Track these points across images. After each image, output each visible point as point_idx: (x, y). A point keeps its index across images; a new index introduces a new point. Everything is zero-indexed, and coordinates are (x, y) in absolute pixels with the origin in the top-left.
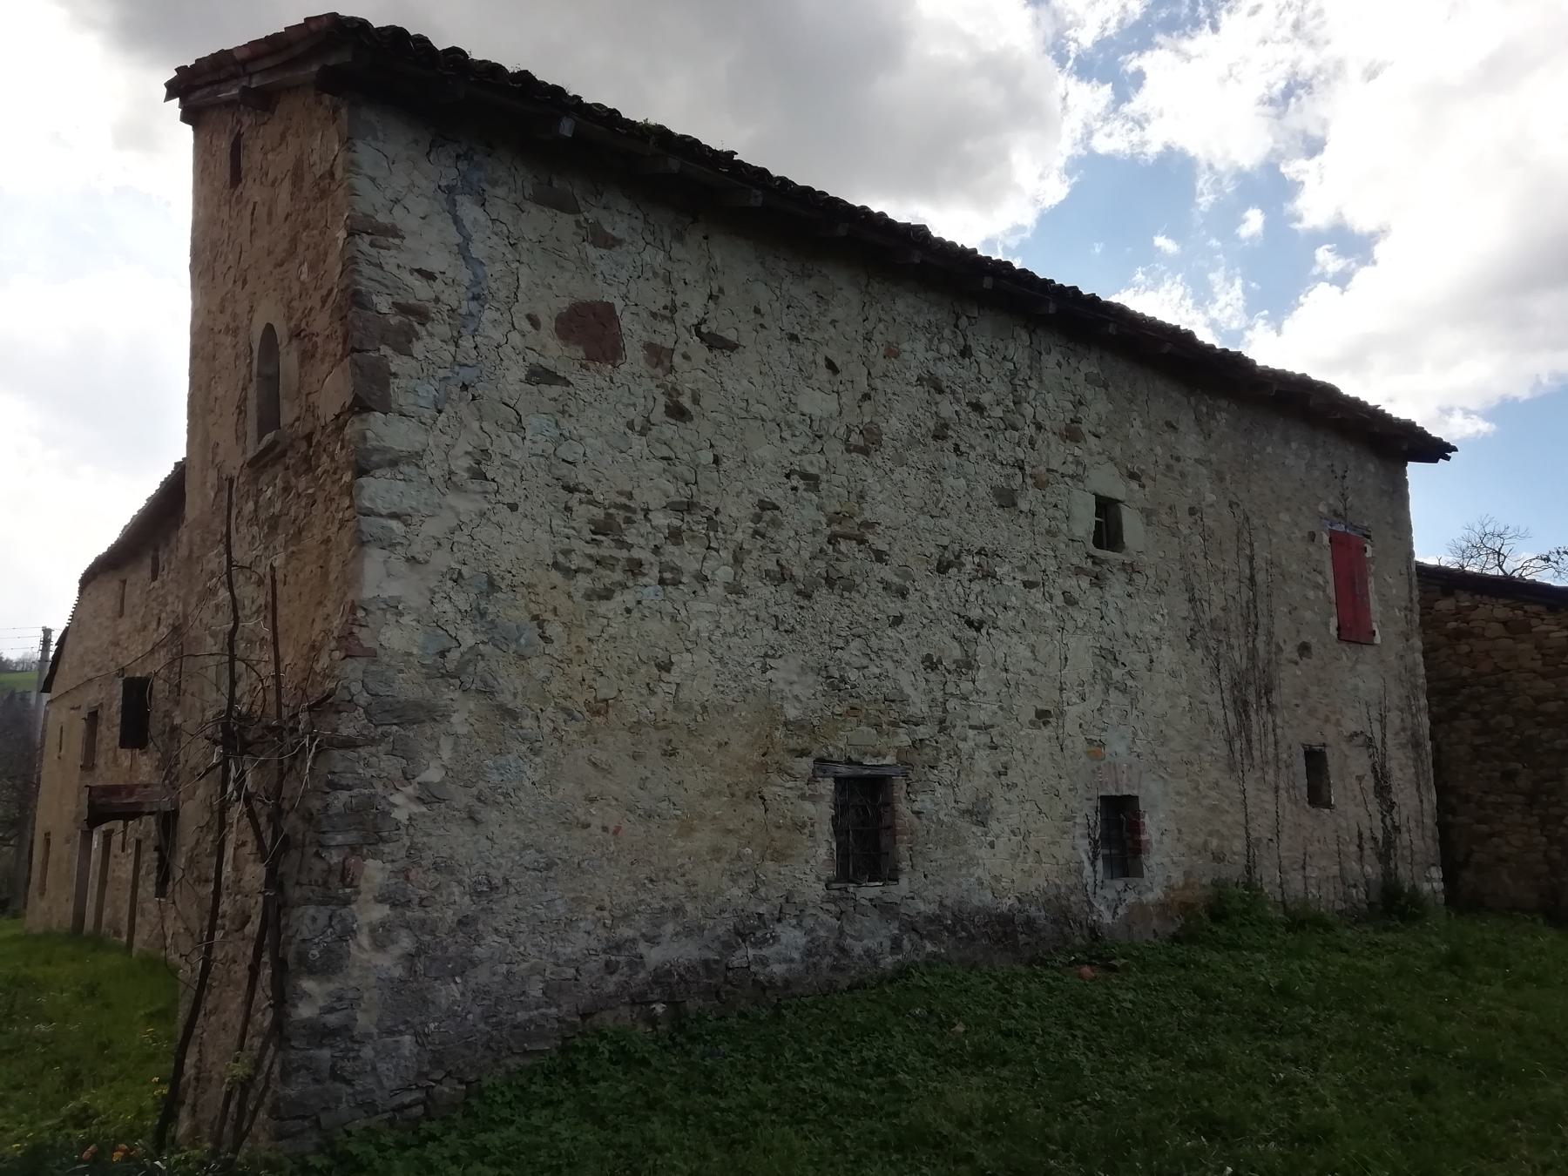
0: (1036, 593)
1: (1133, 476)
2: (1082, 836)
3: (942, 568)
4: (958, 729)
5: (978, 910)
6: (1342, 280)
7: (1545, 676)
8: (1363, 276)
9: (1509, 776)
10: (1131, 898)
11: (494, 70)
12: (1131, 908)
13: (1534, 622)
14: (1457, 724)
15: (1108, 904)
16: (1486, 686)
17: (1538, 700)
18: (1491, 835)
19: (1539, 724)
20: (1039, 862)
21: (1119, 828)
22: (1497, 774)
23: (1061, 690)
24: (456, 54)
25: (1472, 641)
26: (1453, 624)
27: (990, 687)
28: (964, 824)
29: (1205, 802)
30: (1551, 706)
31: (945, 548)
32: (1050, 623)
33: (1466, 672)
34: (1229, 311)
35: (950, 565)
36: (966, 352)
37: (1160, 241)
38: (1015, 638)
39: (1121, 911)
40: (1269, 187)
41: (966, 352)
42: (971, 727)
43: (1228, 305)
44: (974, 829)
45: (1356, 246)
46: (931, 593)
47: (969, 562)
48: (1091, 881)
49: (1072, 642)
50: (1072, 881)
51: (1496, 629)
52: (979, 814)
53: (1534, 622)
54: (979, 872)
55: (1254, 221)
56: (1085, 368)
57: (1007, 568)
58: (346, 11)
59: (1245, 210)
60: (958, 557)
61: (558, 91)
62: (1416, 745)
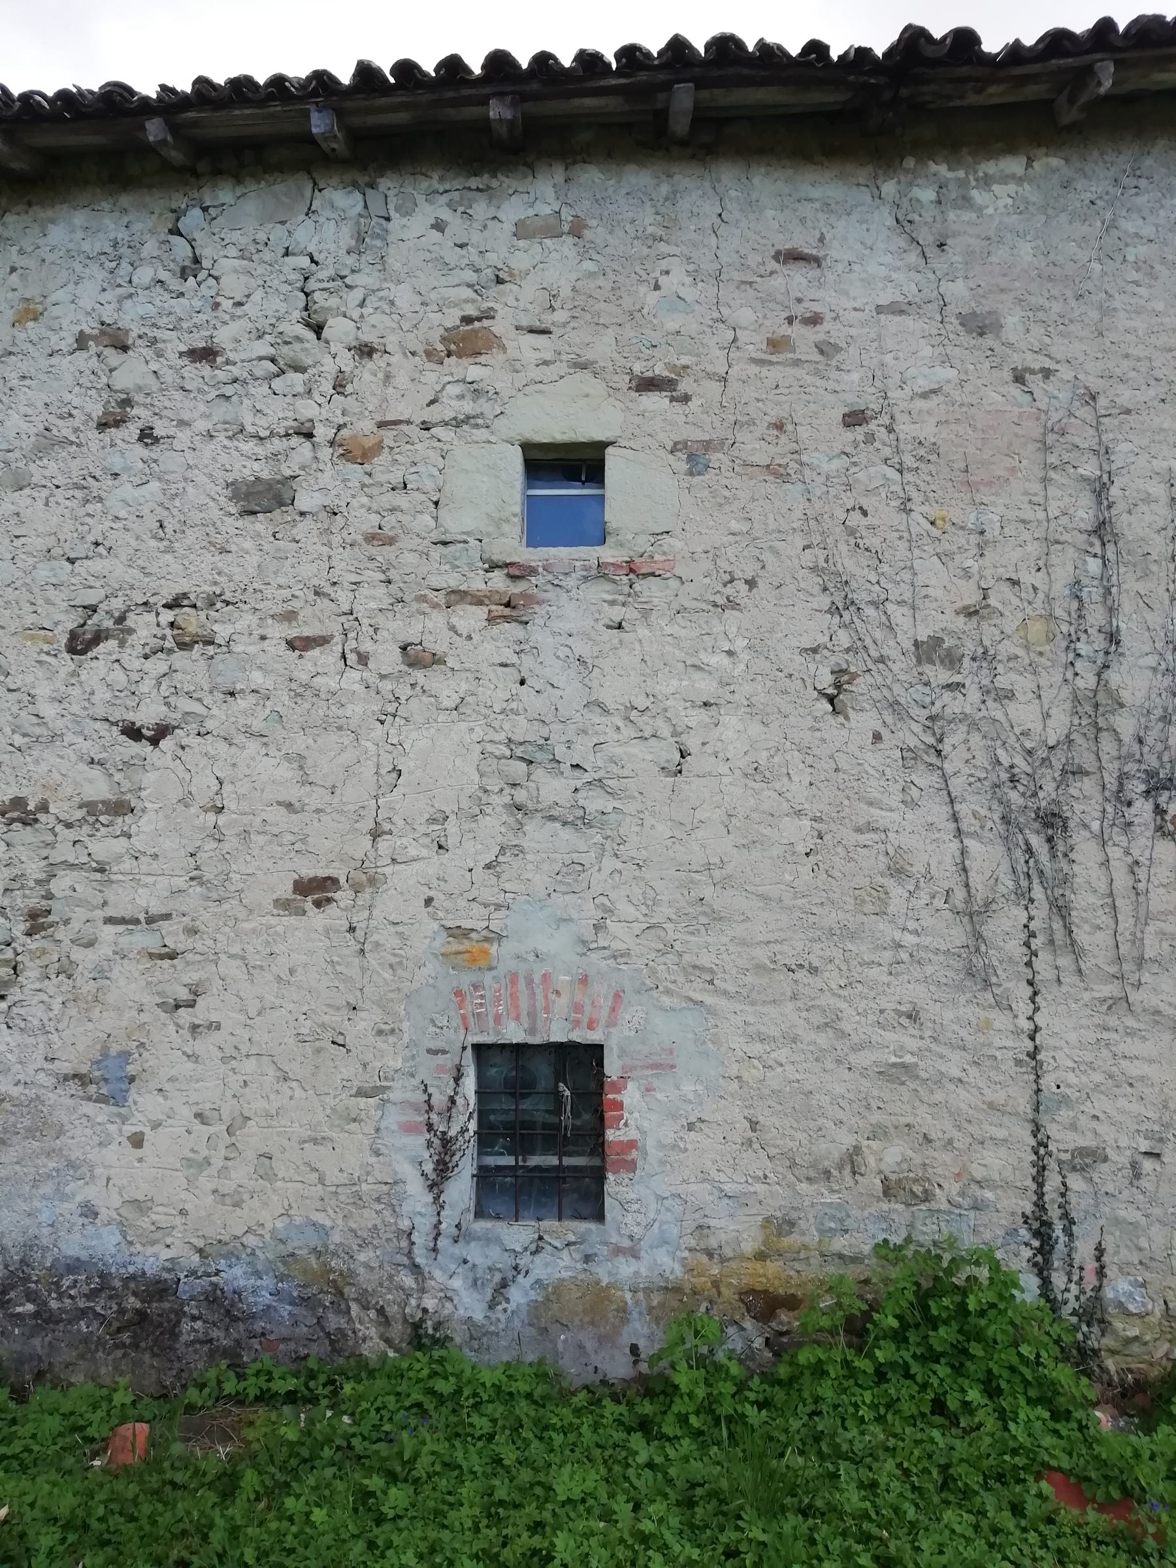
0: (324, 658)
1: (648, 385)
2: (408, 1128)
3: (80, 644)
4: (75, 925)
5: (74, 1266)
10: (556, 1266)
11: (769, 53)
12: (553, 1293)
15: (488, 1277)
20: (269, 1176)
21: (542, 1120)
23: (376, 834)
27: (168, 844)
28: (63, 1103)
29: (864, 1059)
31: (94, 609)
32: (354, 710)
35: (99, 637)
36: (193, 267)
38: (253, 746)
39: (518, 1296)
41: (193, 267)
42: (109, 920)
44: (89, 1108)
46: (43, 690)
47: (144, 627)
48: (424, 1225)
49: (416, 739)
50: (368, 1218)
52: (107, 1080)
54: (91, 1193)
56: (513, 210)
57: (247, 620)
58: (1149, 12)
60: (121, 619)
61: (1058, 41)
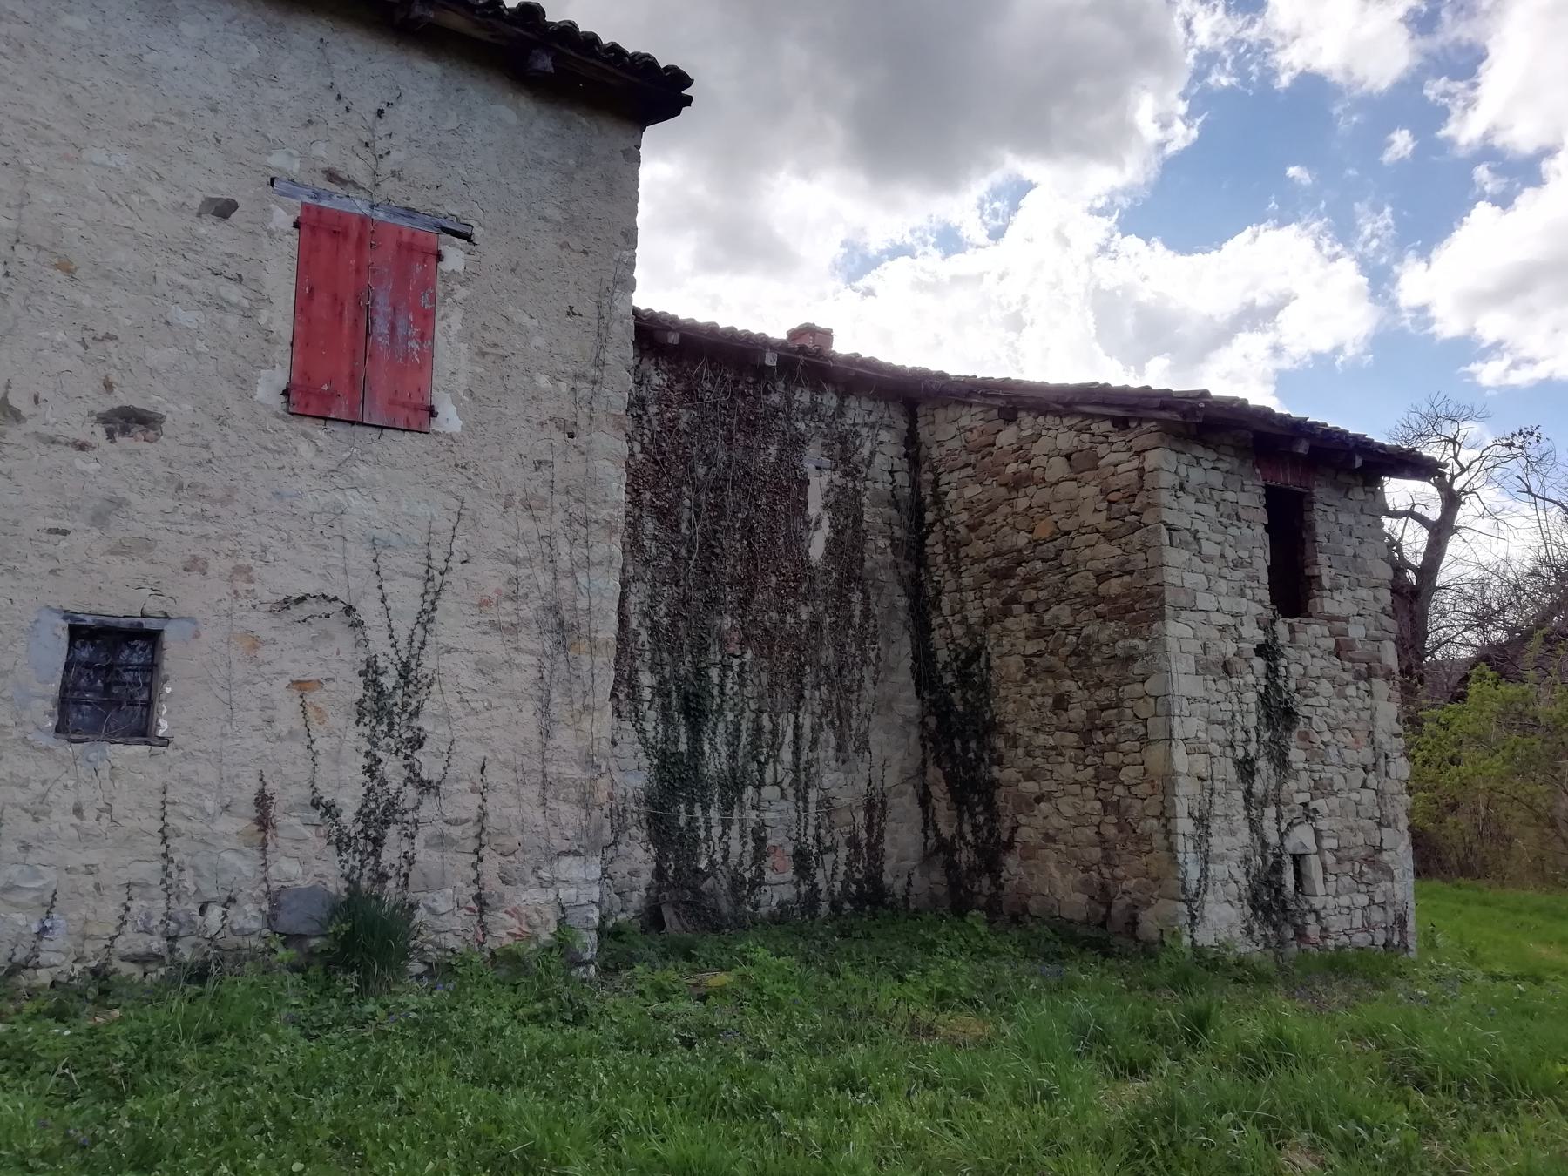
6: (1504, 201)
7: (1108, 537)
8: (1527, 199)
9: (1061, 703)
11: (592, 39)
13: (1102, 450)
14: (1009, 622)
16: (1044, 560)
17: (1102, 577)
18: (1039, 800)
19: (1099, 616)
22: (1050, 701)
24: (614, 48)
25: (1031, 490)
26: (1013, 467)
30: (1114, 586)
33: (1022, 539)
34: (1375, 243)
37: (1292, 171)
40: (1411, 104)
43: (1373, 236)
45: (1521, 172)
51: (1059, 467)
53: (1102, 450)
55: (1402, 142)
59: (1391, 130)
62: (563, 630)
